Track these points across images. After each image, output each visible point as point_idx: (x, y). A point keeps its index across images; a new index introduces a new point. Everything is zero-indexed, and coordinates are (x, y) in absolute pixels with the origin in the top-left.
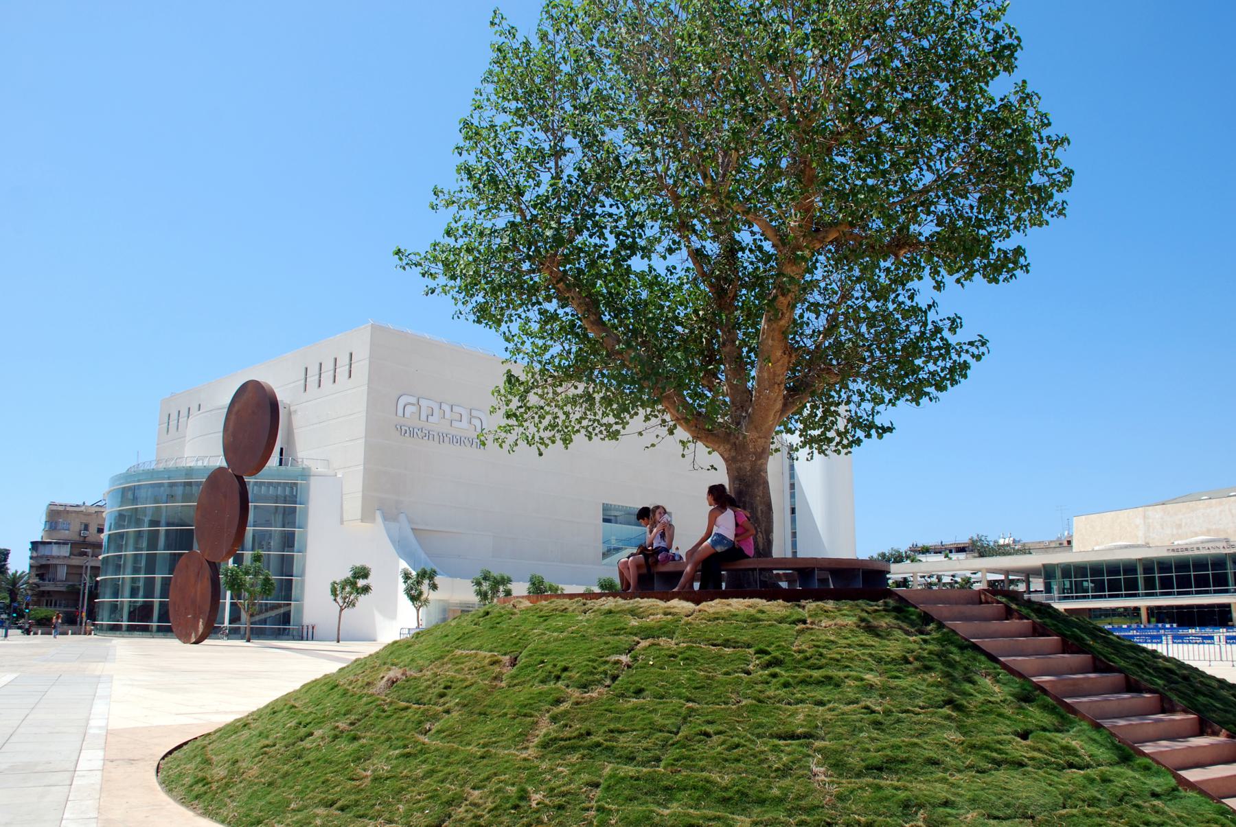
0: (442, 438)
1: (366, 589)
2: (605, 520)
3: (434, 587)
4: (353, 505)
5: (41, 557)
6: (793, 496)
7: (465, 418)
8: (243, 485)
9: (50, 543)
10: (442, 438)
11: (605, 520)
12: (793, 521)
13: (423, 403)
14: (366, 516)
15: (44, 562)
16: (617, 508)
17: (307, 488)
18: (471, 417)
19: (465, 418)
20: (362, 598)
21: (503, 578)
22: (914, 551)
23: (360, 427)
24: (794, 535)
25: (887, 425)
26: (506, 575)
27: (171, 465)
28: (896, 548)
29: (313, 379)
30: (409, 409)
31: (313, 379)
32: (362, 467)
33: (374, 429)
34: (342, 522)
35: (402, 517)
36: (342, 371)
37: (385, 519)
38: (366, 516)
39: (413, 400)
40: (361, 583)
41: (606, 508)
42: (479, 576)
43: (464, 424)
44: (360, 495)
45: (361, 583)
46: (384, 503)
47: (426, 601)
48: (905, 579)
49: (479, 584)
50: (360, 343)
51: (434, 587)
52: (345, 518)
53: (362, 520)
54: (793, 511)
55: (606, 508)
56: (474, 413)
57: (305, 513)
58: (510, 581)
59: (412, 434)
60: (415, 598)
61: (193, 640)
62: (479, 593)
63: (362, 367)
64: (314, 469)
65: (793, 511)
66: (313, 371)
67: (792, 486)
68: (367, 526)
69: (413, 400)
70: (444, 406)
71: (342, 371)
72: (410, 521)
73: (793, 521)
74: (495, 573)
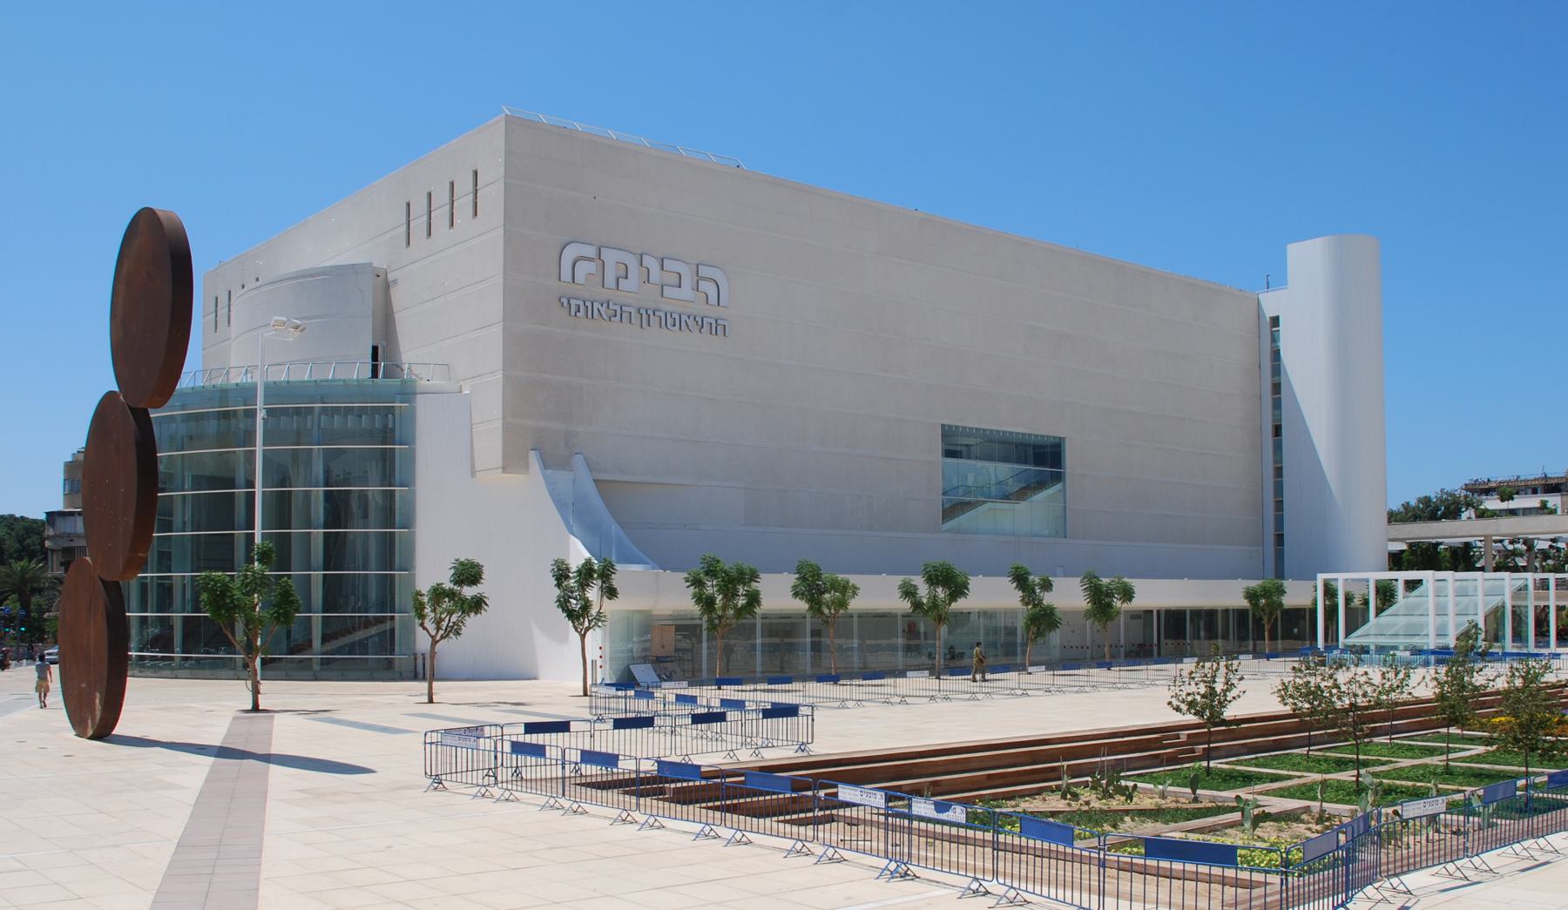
0: (646, 316)
1: (477, 604)
2: (950, 453)
3: (611, 593)
4: (490, 445)
5: (61, 536)
6: (1277, 405)
7: (687, 282)
8: (142, 418)
9: (72, 514)
10: (646, 316)
11: (950, 453)
12: (1278, 448)
13: (610, 256)
14: (512, 461)
15: (66, 545)
16: (968, 432)
17: (411, 416)
18: (699, 278)
19: (687, 282)
20: (472, 620)
21: (741, 573)
22: (1473, 491)
23: (494, 307)
24: (1279, 472)
25: (616, 581)
26: (746, 566)
27: (219, 382)
28: (1448, 489)
29: (419, 224)
30: (584, 269)
31: (419, 224)
32: (500, 375)
33: (517, 303)
34: (473, 473)
35: (578, 461)
36: (464, 203)
37: (546, 464)
38: (512, 461)
39: (590, 252)
40: (468, 592)
41: (948, 433)
42: (698, 568)
43: (686, 291)
44: (499, 424)
45: (468, 592)
46: (545, 434)
47: (599, 617)
48: (1468, 546)
49: (697, 583)
50: (486, 150)
51: (611, 593)
52: (477, 468)
53: (504, 469)
54: (1277, 431)
55: (948, 433)
56: (704, 271)
57: (411, 458)
58: (754, 576)
59: (590, 315)
60: (578, 615)
61: (90, 732)
62: (699, 599)
63: (493, 196)
64: (422, 384)
65: (1277, 431)
66: (419, 209)
67: (1277, 388)
68: (514, 479)
69: (590, 252)
70: (647, 261)
71: (464, 203)
72: (591, 469)
73: (1278, 448)
74: (728, 564)
